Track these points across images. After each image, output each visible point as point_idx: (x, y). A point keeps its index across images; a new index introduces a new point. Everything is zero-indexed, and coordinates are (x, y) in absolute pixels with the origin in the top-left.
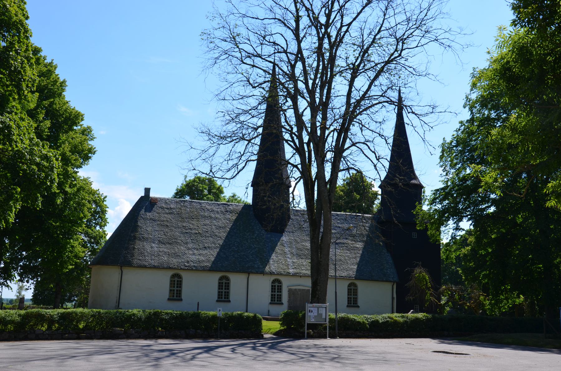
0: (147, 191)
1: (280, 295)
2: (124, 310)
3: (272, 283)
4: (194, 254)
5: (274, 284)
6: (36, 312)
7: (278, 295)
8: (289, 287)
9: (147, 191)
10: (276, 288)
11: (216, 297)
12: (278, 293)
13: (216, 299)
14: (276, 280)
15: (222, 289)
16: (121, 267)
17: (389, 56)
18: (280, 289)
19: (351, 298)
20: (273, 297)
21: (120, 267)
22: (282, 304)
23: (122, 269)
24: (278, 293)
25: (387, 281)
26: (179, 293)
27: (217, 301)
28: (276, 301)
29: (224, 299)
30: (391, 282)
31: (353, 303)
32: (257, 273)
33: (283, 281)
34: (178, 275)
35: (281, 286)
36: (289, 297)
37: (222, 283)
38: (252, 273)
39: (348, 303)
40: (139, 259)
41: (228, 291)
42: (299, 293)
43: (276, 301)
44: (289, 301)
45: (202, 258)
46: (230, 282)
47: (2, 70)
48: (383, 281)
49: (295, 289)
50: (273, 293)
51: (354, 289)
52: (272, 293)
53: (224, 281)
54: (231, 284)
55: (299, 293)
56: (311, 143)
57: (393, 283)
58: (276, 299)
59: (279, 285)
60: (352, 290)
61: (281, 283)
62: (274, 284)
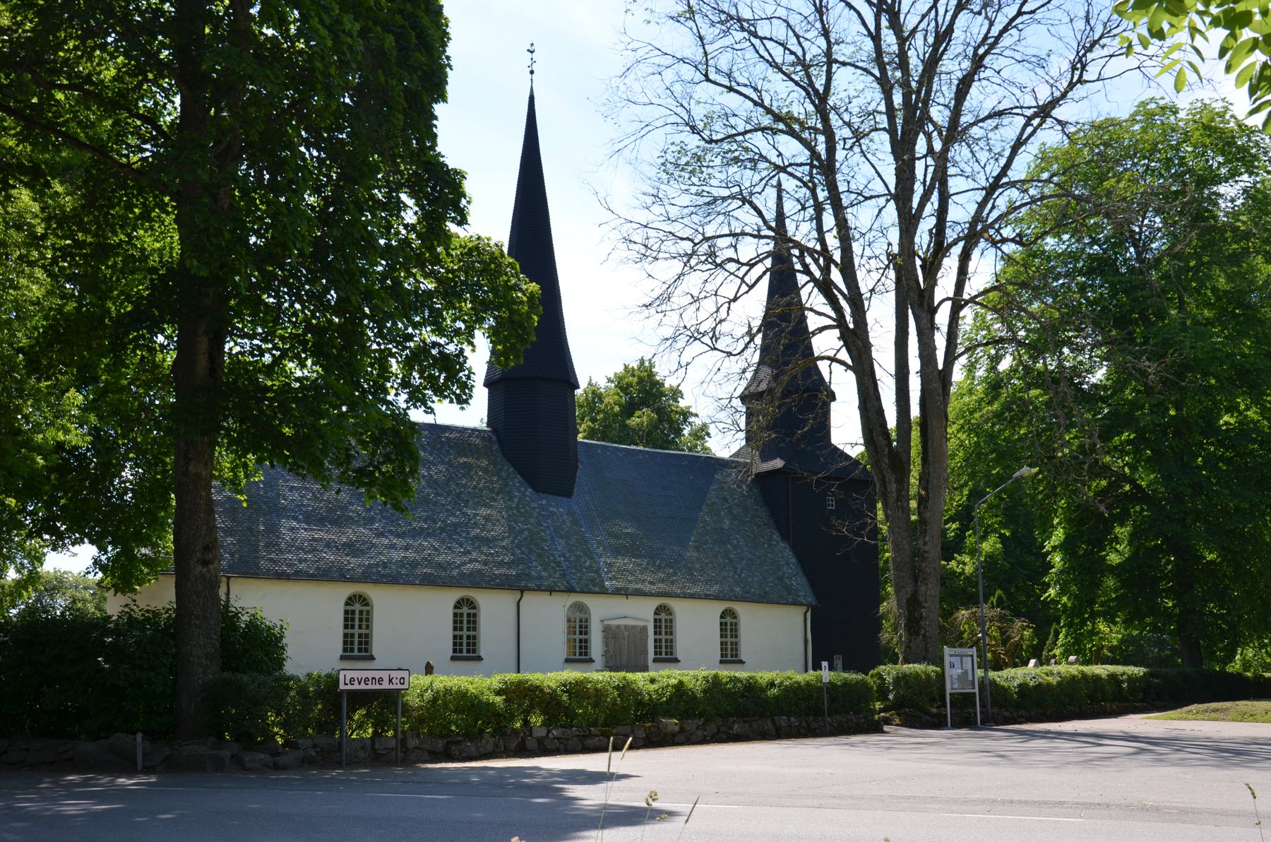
1: (586, 641)
2: (691, 672)
4: (393, 546)
5: (350, 608)
7: (468, 637)
8: (606, 623)
10: (465, 619)
12: (469, 633)
13: (340, 652)
14: (463, 599)
15: (461, 629)
17: (825, 68)
18: (584, 628)
19: (352, 635)
20: (348, 640)
22: (591, 661)
24: (469, 633)
25: (795, 603)
27: (453, 659)
28: (356, 650)
30: (801, 604)
31: (730, 655)
32: (539, 589)
34: (360, 596)
35: (475, 615)
36: (606, 644)
37: (462, 615)
38: (529, 589)
39: (345, 650)
40: (271, 560)
42: (626, 633)
43: (356, 650)
45: (410, 554)
46: (372, 608)
47: (895, 443)
48: (787, 604)
49: (618, 627)
50: (458, 633)
52: (347, 631)
53: (465, 610)
55: (626, 633)
57: (804, 609)
58: (356, 646)
59: (472, 611)
61: (474, 608)
62: (350, 608)
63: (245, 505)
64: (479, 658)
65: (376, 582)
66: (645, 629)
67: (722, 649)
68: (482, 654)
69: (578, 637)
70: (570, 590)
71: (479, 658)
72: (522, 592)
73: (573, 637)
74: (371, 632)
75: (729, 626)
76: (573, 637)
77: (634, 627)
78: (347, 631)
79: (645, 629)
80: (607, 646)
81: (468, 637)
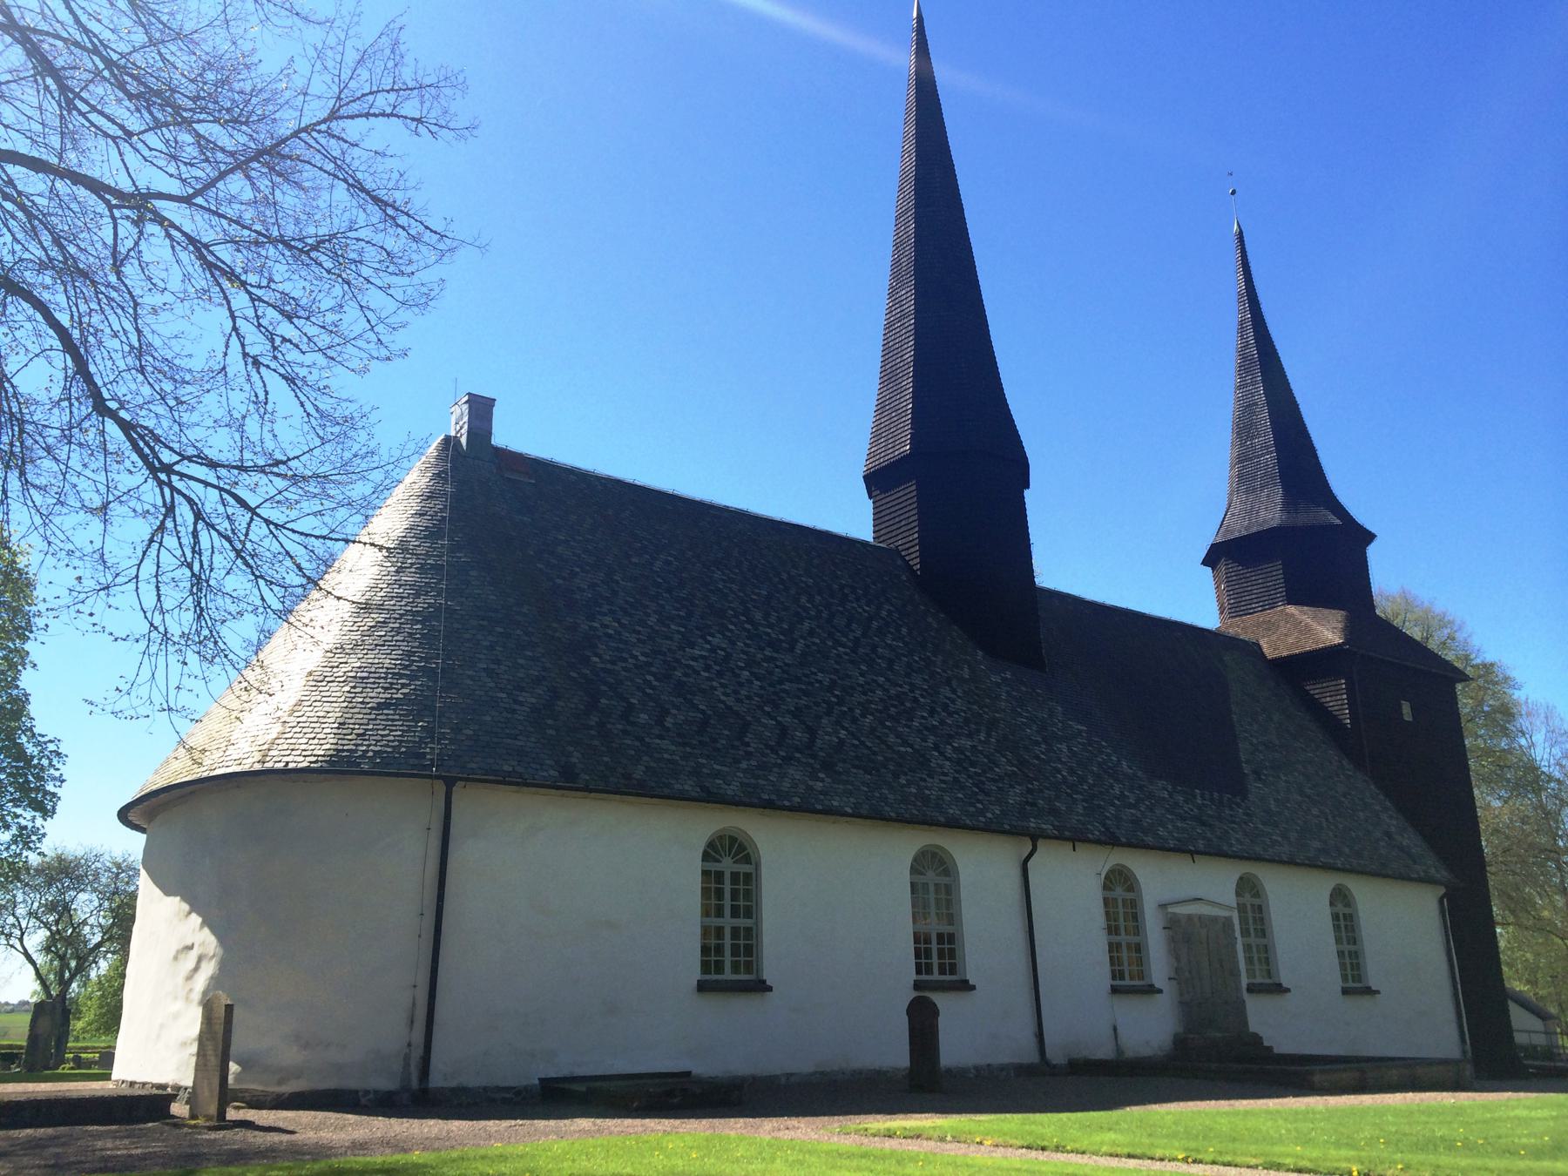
0: (481, 409)
3: (706, 857)
6: (287, 1142)
7: (735, 932)
9: (481, 409)
11: (691, 969)
13: (696, 974)
16: (450, 783)
20: (710, 955)
21: (440, 787)
23: (454, 798)
26: (747, 945)
27: (702, 987)
29: (940, 973)
33: (1141, 880)
36: (1175, 953)
39: (705, 967)
41: (747, 922)
44: (1177, 977)
46: (758, 866)
49: (1190, 917)
51: (735, 877)
54: (1272, 909)
56: (1338, 522)
59: (743, 868)
60: (932, 888)
61: (747, 859)
63: (1349, 726)
64: (761, 987)
65: (769, 805)
66: (1228, 920)
67: (918, 955)
68: (768, 975)
69: (728, 922)
70: (1111, 840)
71: (761, 987)
72: (1034, 839)
73: (715, 922)
74: (758, 923)
75: (1345, 923)
76: (715, 922)
77: (1214, 919)
78: (747, 922)
79: (1228, 920)
80: (1178, 959)
81: (735, 932)
